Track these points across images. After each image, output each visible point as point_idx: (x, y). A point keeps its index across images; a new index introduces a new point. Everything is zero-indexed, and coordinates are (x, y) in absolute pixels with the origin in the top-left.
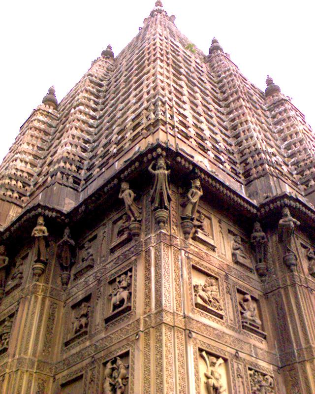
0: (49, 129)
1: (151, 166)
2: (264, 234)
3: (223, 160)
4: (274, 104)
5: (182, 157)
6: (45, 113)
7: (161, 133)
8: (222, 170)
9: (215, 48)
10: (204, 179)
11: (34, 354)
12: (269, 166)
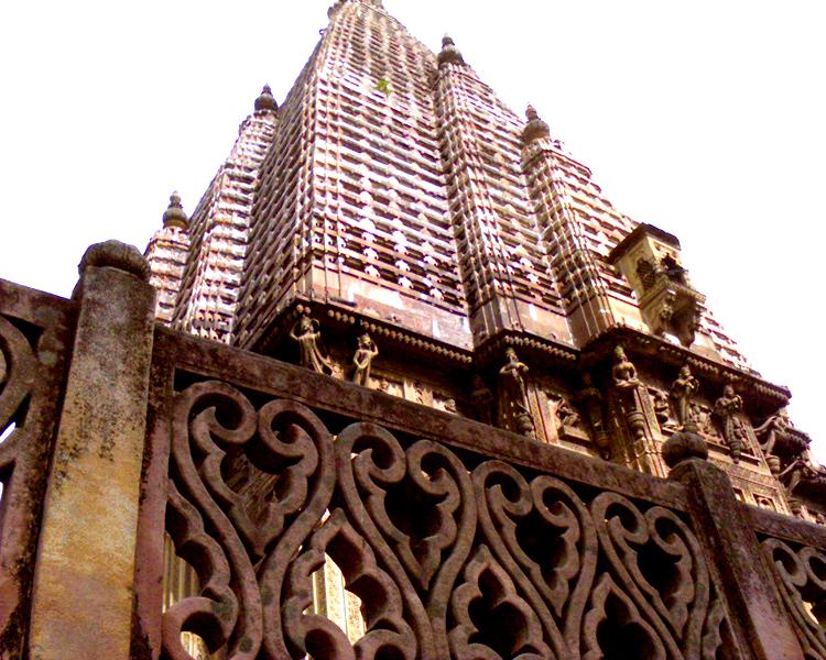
0: (177, 268)
1: (293, 330)
2: (487, 390)
3: (429, 284)
4: (532, 160)
5: (336, 309)
6: (167, 244)
7: (315, 272)
8: (427, 302)
9: (449, 57)
10: (376, 331)
12: (500, 280)
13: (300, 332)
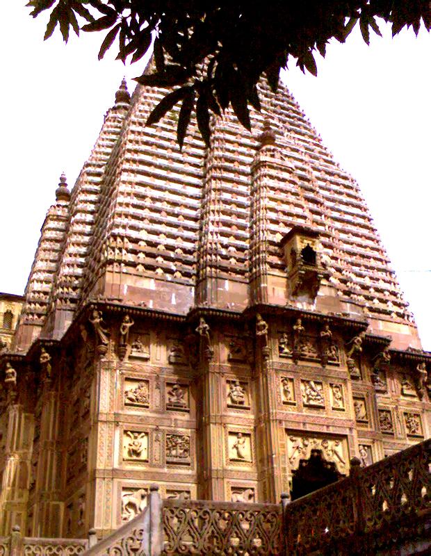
11: (53, 437)
13: (93, 318)
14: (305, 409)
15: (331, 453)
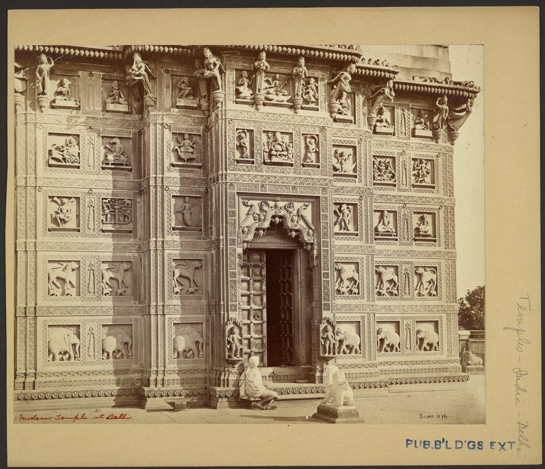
14: (265, 167)
15: (296, 218)
